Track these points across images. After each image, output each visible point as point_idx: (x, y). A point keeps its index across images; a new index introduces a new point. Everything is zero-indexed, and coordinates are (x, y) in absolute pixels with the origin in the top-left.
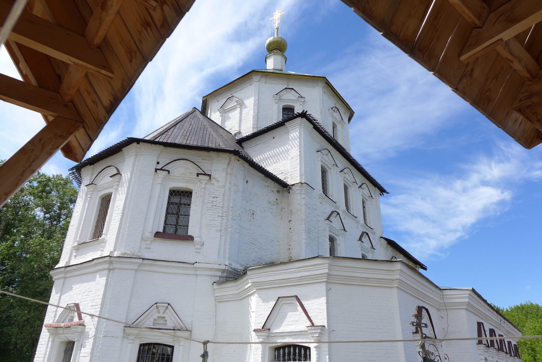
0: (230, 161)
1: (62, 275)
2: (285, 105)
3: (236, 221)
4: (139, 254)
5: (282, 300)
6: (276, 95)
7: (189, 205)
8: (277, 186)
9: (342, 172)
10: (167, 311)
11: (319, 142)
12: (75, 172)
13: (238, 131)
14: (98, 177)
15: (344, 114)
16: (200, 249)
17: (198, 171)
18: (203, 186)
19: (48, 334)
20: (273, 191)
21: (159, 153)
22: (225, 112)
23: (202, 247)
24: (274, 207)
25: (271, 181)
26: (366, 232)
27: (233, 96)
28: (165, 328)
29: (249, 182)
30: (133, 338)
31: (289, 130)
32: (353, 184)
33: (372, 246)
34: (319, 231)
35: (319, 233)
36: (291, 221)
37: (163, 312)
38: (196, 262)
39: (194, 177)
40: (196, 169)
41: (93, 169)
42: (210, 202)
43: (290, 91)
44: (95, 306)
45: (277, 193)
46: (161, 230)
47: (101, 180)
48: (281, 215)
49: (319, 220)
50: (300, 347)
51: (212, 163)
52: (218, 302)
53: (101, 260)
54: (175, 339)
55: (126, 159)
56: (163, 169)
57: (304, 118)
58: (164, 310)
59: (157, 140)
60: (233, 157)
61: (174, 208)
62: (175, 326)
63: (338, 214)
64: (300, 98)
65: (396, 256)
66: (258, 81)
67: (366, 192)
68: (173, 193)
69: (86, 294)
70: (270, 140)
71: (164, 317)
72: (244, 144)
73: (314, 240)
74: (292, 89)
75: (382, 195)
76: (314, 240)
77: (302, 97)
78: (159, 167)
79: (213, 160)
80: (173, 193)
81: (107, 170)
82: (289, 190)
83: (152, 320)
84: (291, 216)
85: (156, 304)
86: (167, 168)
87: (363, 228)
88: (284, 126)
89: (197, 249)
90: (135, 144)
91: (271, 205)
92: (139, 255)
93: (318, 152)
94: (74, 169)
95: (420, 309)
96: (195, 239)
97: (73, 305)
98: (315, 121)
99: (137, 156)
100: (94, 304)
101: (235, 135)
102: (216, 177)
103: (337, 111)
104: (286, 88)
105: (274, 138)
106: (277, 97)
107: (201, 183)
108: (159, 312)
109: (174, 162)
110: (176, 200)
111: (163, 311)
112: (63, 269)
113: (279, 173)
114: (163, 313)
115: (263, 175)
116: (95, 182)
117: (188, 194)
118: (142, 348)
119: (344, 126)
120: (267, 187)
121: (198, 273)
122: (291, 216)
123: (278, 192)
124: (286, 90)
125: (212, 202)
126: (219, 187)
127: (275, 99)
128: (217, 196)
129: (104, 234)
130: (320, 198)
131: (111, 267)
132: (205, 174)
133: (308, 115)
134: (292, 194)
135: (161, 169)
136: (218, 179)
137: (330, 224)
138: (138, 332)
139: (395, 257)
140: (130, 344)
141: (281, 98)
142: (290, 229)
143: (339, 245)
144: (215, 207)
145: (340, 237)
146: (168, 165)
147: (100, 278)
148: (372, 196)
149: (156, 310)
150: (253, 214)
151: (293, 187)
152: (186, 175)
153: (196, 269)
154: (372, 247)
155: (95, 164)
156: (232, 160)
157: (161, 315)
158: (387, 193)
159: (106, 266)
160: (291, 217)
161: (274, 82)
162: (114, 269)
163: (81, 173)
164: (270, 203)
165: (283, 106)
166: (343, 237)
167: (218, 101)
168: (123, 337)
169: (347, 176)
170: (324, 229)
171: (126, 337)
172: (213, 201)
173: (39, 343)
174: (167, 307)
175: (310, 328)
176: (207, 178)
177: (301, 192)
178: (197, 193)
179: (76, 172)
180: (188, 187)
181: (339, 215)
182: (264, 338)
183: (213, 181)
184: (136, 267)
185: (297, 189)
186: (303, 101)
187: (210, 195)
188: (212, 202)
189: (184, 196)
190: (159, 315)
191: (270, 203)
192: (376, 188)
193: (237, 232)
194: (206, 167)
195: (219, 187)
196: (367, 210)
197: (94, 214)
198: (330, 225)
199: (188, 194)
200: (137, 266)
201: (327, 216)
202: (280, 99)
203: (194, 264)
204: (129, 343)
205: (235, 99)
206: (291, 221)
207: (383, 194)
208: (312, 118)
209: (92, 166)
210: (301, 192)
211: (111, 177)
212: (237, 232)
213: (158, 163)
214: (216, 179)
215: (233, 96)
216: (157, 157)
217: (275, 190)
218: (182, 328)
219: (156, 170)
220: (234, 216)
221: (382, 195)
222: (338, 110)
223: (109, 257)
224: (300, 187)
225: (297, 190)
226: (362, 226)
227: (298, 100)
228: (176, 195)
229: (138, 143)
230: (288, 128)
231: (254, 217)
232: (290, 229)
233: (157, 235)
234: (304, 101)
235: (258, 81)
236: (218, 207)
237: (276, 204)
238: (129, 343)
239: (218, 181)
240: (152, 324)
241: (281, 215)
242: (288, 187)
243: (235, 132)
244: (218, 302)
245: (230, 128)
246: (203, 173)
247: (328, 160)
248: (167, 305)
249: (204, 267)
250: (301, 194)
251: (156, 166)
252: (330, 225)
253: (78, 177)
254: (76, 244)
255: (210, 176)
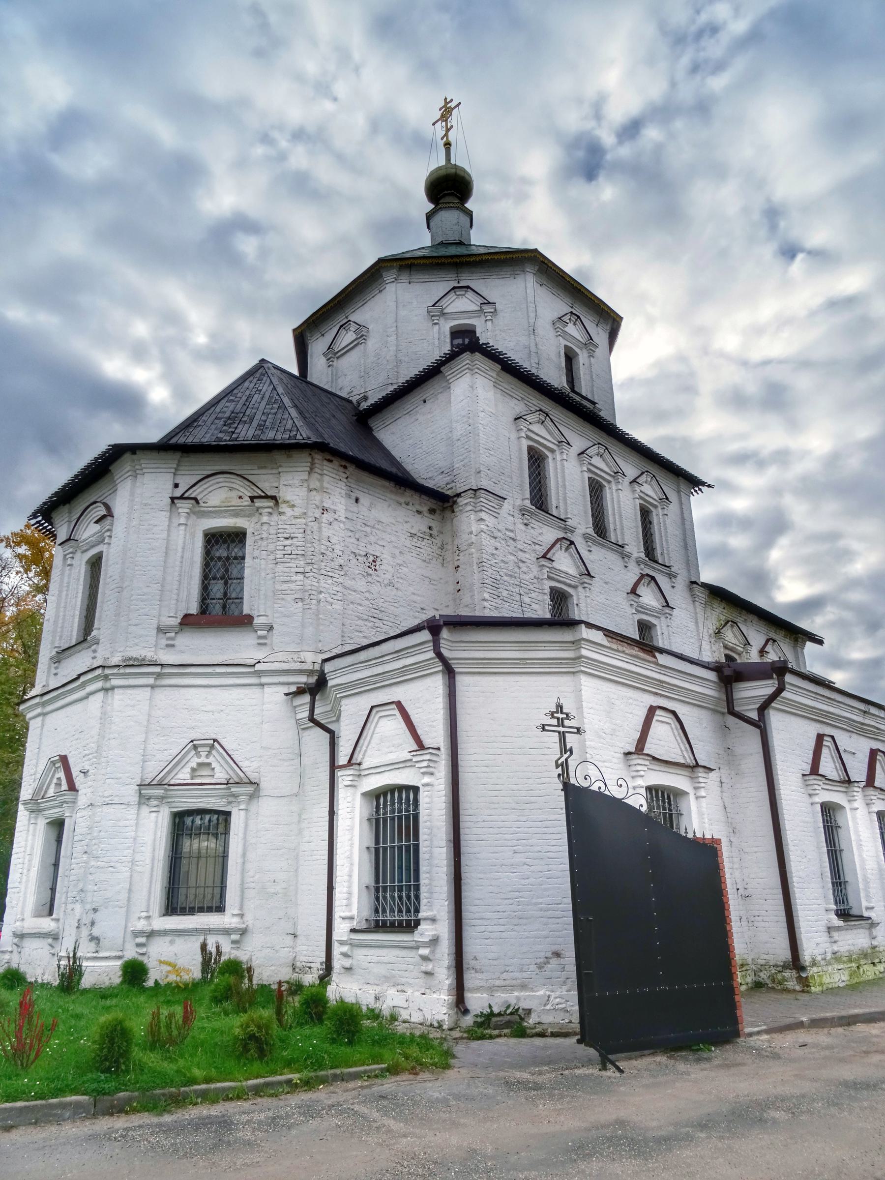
0: (313, 464)
1: (39, 710)
2: (459, 324)
3: (334, 579)
4: (155, 658)
5: (377, 712)
6: (433, 306)
7: (243, 558)
8: (426, 504)
9: (582, 456)
10: (214, 752)
11: (520, 399)
12: (41, 521)
13: (363, 395)
14: (79, 526)
15: (597, 325)
16: (264, 637)
17: (252, 491)
18: (265, 519)
19: (27, 813)
20: (419, 512)
21: (175, 466)
22: (338, 358)
23: (270, 633)
24: (423, 543)
25: (412, 492)
26: (647, 575)
27: (350, 321)
28: (213, 781)
29: (361, 500)
30: (155, 803)
31: (450, 381)
32: (614, 477)
33: (666, 601)
34: (522, 581)
35: (522, 585)
36: (458, 567)
37: (207, 755)
38: (259, 662)
39: (246, 503)
40: (249, 489)
41: (70, 512)
42: (278, 548)
43: (463, 293)
44: (89, 755)
45: (428, 515)
46: (194, 609)
47: (85, 530)
48: (441, 558)
49: (524, 560)
50: (408, 788)
51: (280, 473)
52: (303, 729)
53: (90, 676)
54: (231, 799)
55: (119, 485)
56: (186, 495)
57: (477, 353)
58: (209, 752)
59: (173, 441)
60: (318, 457)
61: (218, 568)
62: (229, 777)
63: (572, 543)
64: (484, 307)
65: (735, 620)
66: (393, 282)
67: (649, 490)
68: (213, 539)
69: (76, 737)
70: (419, 408)
71: (209, 764)
72: (374, 423)
73: (510, 601)
74: (468, 287)
75: (699, 492)
76: (510, 601)
77: (489, 303)
78: (178, 493)
79: (280, 466)
80: (213, 539)
81: (90, 512)
82: (452, 506)
83: (187, 770)
84: (459, 558)
85: (192, 741)
86: (192, 493)
87: (642, 566)
88: (441, 375)
89: (260, 637)
90: (127, 456)
91: (415, 540)
92: (154, 659)
93: (517, 421)
94: (39, 516)
95: (820, 738)
96: (257, 621)
97: (57, 758)
98: (503, 355)
99: (136, 477)
100: (87, 752)
101: (359, 403)
102: (288, 498)
103: (576, 320)
104: (454, 288)
105: (425, 402)
106: (436, 311)
107: (261, 514)
108: (198, 754)
109: (206, 480)
110: (221, 552)
111: (207, 753)
112: (37, 700)
113: (436, 474)
114: (207, 756)
115: (392, 484)
116: (74, 535)
117: (238, 537)
118: (177, 820)
119: (594, 352)
120: (404, 505)
121: (264, 680)
122: (459, 558)
123: (432, 511)
124: (455, 292)
125: (282, 548)
126: (296, 517)
127: (432, 316)
128: (292, 535)
129: (96, 629)
130: (523, 514)
131: (108, 685)
132: (267, 497)
133: (483, 344)
134: (457, 514)
135: (182, 497)
136: (293, 503)
137: (550, 566)
138: (163, 791)
139: (732, 621)
140: (154, 815)
141: (445, 311)
142: (458, 583)
143: (577, 605)
144: (290, 557)
145: (580, 589)
146: (194, 488)
147: (720, 839)
148: (667, 499)
149: (193, 752)
150: (374, 561)
151: (459, 500)
152: (229, 502)
153: (259, 674)
154: (665, 604)
155: (72, 502)
156: (316, 461)
157: (203, 759)
158: (709, 486)
159: (99, 685)
160: (458, 560)
161: (427, 277)
162: (113, 688)
163: (52, 520)
164: (413, 535)
165: (451, 328)
166: (587, 589)
167: (410, 283)
168: (140, 804)
169: (597, 461)
170: (535, 577)
171: (144, 804)
172: (285, 546)
173: (17, 830)
174: (213, 745)
175: (415, 753)
176: (271, 503)
177: (475, 507)
178: (256, 534)
179: (43, 521)
180: (237, 525)
181: (573, 546)
182: (351, 778)
183: (283, 508)
184: (151, 681)
185: (466, 501)
186: (492, 310)
187: (279, 535)
188: (282, 548)
189: (233, 541)
190: (200, 761)
191: (413, 535)
192: (680, 478)
193: (338, 600)
194: (267, 483)
195: (296, 517)
196: (656, 528)
197: (80, 595)
198: (549, 568)
199: (238, 537)
200: (153, 679)
201: (541, 550)
202: (444, 314)
203: (254, 665)
204: (150, 812)
205: (353, 327)
206: (458, 567)
207: (700, 490)
208: (493, 350)
209: (67, 506)
210: (475, 507)
211: (96, 522)
212: (338, 600)
213: (176, 486)
214: (288, 502)
215: (350, 321)
216: (172, 475)
217: (425, 509)
218: (241, 779)
219: (173, 499)
220: (330, 570)
221: (699, 492)
222: (579, 317)
223: (101, 668)
224: (471, 498)
225: (466, 504)
226: (638, 562)
227: (481, 310)
228: (217, 542)
229: (134, 453)
230: (448, 378)
231: (377, 568)
232: (458, 583)
233: (188, 622)
234: (496, 310)
235: (393, 282)
236: (295, 557)
237: (428, 538)
238: (150, 812)
239: (293, 506)
240: (188, 776)
241: (441, 558)
242: (451, 500)
243: (358, 397)
244: (303, 729)
245: (347, 389)
246: (263, 494)
247: (543, 433)
248: (212, 742)
249: (273, 668)
250: (476, 512)
251: (173, 493)
252: (549, 568)
253: (47, 526)
254: (54, 653)
255: (274, 498)
